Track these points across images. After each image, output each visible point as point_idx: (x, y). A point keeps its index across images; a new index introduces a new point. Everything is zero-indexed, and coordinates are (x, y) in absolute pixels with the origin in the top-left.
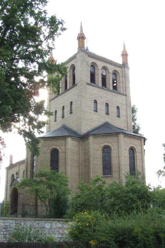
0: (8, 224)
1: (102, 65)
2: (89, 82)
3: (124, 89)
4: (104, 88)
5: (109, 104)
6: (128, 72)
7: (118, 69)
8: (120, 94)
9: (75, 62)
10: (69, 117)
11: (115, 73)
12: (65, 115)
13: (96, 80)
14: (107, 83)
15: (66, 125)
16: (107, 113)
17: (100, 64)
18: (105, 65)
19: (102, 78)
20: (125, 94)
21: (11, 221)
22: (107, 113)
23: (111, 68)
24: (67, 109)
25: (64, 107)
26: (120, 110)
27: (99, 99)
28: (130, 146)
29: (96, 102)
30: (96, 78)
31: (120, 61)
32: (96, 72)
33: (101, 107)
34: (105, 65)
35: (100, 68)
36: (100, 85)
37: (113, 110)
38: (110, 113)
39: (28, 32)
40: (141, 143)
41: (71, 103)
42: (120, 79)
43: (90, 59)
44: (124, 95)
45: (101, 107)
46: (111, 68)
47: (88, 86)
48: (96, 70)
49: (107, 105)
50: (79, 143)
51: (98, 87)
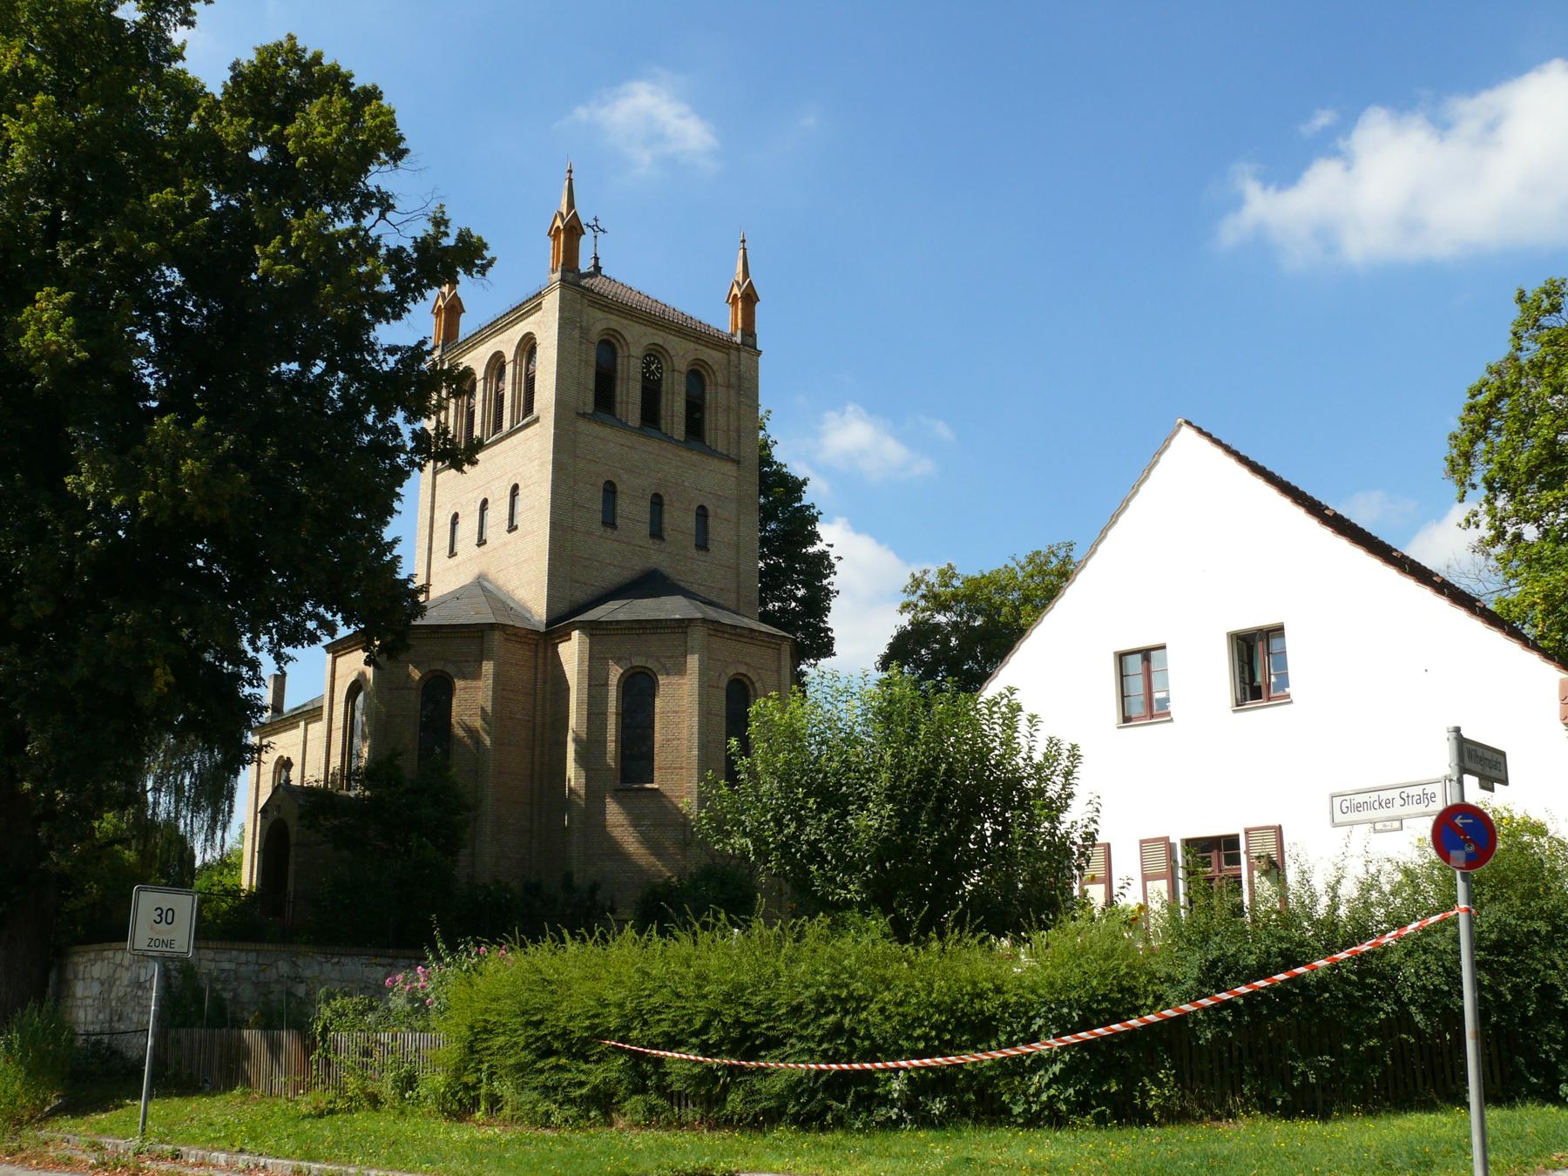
0: (233, 966)
1: (646, 341)
2: (590, 409)
3: (733, 435)
4: (602, 416)
5: (666, 499)
6: (755, 368)
7: (713, 357)
8: (712, 453)
9: (538, 324)
10: (505, 545)
11: (697, 376)
12: (489, 534)
13: (618, 399)
14: (663, 413)
15: (491, 577)
16: (657, 533)
17: (637, 339)
18: (613, 325)
19: (644, 389)
20: (733, 453)
21: (243, 957)
22: (657, 533)
23: (682, 353)
24: (498, 514)
25: (485, 502)
26: (711, 521)
27: (625, 476)
28: (731, 672)
29: (610, 490)
30: (618, 389)
31: (724, 321)
32: (619, 367)
33: (633, 510)
34: (659, 338)
35: (637, 351)
36: (679, 431)
37: (679, 520)
38: (668, 532)
39: (123, 147)
40: (779, 660)
41: (515, 488)
42: (717, 396)
43: (599, 314)
44: (733, 461)
45: (633, 510)
46: (682, 353)
47: (583, 426)
48: (619, 360)
49: (657, 502)
50: (536, 652)
51: (624, 426)
